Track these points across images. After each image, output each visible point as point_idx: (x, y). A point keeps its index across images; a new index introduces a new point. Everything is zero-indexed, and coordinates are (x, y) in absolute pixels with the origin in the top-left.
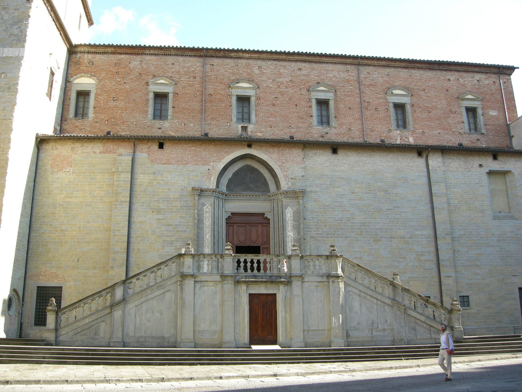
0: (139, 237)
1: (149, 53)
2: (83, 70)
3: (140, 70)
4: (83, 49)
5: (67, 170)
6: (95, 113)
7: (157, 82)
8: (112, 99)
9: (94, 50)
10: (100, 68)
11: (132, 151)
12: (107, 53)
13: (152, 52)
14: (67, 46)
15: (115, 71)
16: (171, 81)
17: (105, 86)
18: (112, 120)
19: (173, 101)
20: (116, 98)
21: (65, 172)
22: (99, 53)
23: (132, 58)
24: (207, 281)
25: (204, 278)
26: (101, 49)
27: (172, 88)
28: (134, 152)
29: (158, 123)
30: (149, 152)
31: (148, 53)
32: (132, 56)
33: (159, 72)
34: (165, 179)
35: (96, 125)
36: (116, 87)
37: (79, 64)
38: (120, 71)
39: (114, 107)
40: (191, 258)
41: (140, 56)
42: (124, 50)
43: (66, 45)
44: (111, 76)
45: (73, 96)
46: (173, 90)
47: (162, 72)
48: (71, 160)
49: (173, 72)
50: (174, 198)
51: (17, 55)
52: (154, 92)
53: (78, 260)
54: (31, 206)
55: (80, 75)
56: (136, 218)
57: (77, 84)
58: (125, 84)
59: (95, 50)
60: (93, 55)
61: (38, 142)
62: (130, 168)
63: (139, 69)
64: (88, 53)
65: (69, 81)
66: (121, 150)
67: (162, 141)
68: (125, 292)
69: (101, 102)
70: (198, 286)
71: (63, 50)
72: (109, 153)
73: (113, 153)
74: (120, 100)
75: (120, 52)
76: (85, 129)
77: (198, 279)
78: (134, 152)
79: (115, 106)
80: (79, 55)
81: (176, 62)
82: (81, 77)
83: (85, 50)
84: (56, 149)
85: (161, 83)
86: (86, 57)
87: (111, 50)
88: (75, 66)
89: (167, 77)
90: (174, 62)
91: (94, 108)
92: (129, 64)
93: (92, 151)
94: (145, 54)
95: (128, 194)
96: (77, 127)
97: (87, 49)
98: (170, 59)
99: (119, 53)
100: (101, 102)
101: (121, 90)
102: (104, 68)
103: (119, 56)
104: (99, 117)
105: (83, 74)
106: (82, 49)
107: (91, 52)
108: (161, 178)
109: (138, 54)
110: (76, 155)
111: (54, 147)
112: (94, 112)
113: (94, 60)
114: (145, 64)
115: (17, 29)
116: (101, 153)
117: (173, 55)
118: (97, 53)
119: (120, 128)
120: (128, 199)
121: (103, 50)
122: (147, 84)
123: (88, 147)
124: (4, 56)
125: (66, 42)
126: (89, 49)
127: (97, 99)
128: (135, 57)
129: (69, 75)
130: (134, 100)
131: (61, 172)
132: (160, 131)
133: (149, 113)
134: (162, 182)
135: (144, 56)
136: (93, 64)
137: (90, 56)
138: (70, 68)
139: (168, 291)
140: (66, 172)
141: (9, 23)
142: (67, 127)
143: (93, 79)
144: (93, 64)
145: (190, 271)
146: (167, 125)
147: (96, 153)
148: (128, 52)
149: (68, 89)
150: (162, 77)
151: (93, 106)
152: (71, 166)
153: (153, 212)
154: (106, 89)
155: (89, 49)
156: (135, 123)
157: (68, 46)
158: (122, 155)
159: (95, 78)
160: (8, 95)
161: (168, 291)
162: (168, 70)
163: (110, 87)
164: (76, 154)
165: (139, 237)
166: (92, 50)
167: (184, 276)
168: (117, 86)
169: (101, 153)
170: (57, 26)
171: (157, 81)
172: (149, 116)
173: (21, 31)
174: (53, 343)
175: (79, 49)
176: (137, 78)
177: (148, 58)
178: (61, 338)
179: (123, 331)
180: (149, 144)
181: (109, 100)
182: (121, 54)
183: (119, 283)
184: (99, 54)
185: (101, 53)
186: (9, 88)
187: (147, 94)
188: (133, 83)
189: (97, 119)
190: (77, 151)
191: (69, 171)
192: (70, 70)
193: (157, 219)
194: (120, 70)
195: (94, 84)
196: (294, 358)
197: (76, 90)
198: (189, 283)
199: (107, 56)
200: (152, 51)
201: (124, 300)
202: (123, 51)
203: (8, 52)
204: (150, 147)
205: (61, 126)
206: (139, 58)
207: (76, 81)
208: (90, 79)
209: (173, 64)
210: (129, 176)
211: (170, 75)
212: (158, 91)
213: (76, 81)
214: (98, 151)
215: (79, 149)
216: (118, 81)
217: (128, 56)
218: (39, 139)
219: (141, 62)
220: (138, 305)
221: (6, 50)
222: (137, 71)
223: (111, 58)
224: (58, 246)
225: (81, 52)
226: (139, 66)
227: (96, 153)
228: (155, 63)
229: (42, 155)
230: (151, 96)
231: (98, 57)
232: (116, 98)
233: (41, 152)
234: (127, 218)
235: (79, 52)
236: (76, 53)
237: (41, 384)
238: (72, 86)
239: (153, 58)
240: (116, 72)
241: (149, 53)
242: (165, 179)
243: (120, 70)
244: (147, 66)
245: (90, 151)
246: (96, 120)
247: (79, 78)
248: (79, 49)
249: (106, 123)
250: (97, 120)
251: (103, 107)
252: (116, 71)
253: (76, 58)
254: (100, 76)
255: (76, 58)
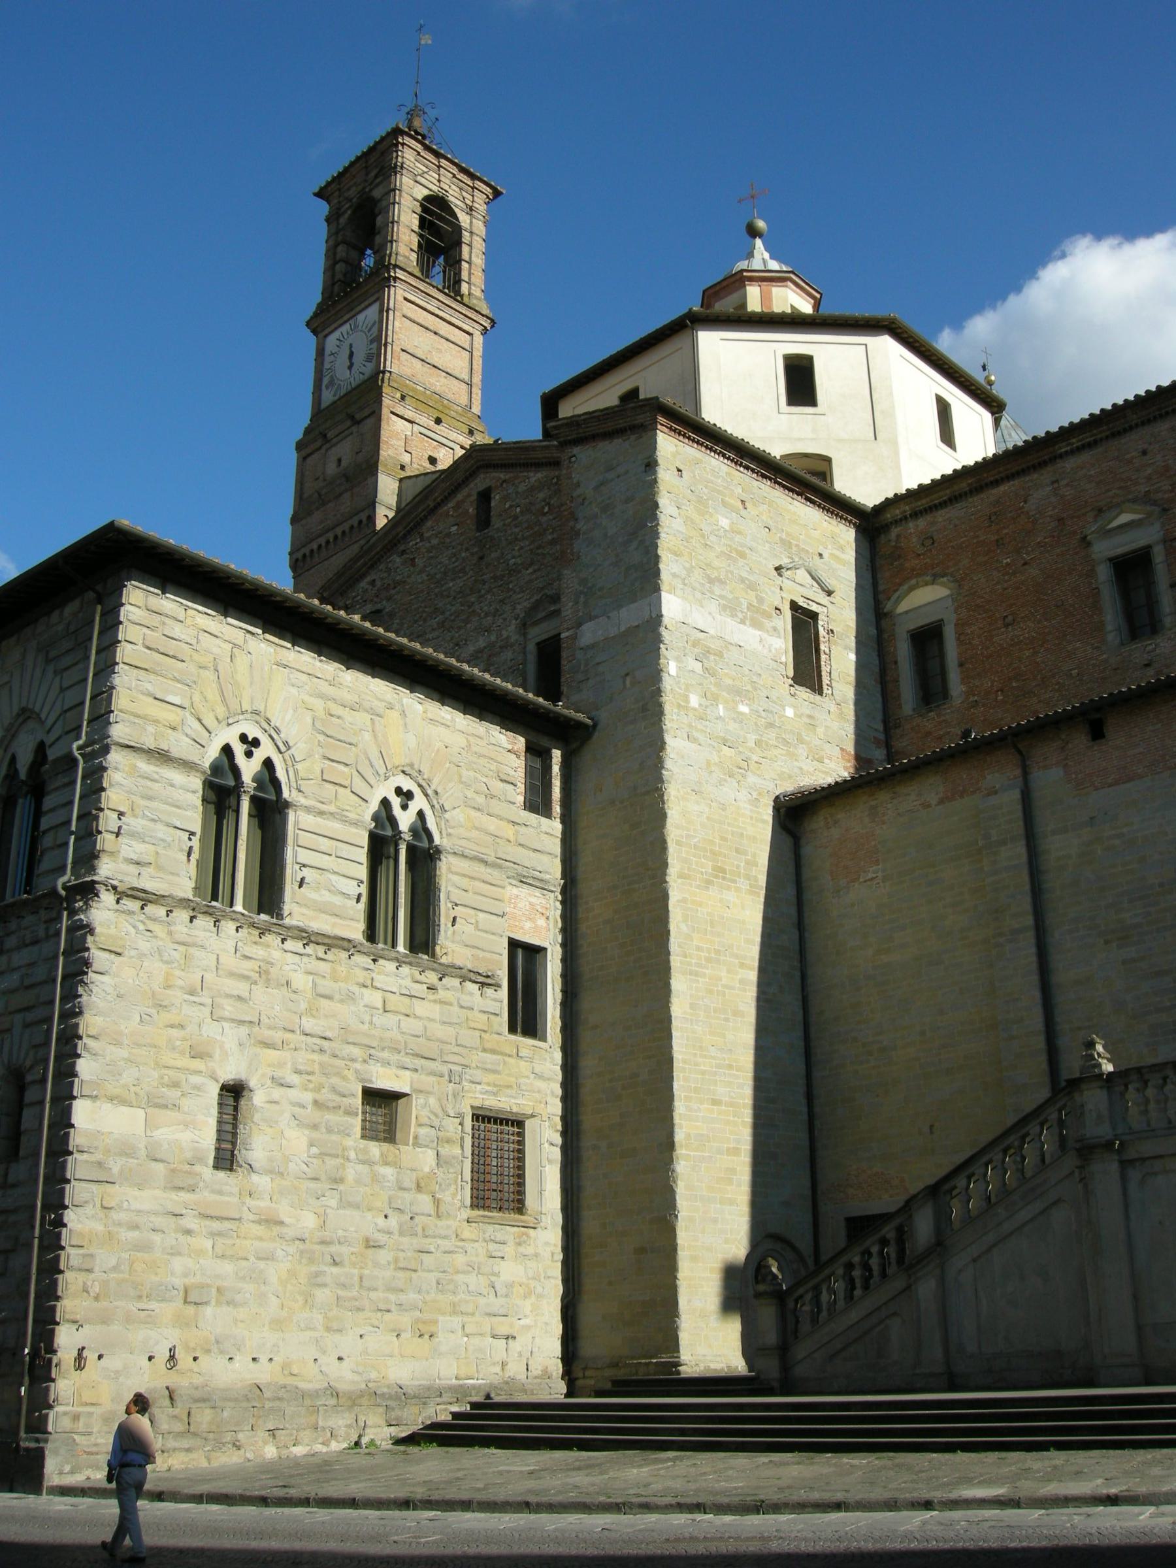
0: (1079, 1028)
1: (1069, 448)
2: (913, 570)
3: (1057, 511)
4: (897, 512)
5: (870, 875)
6: (965, 680)
7: (1111, 526)
8: (1000, 622)
9: (924, 501)
10: (953, 547)
11: (1018, 772)
12: (961, 496)
13: (1075, 442)
14: (850, 522)
15: (994, 538)
16: (1149, 508)
17: (976, 592)
18: (1014, 684)
19: (1168, 565)
20: (1010, 618)
21: (865, 881)
22: (940, 504)
23: (1030, 484)
24: (1161, 1157)
25: (1147, 1148)
26: (941, 494)
27: (1157, 526)
28: (1025, 774)
29: (1138, 651)
30: (1066, 759)
31: (1066, 452)
32: (1027, 479)
33: (1111, 494)
34: (1125, 830)
35: (974, 713)
36: (1005, 585)
37: (899, 556)
38: (1007, 534)
39: (1012, 645)
40: (1101, 1088)
41: (1050, 468)
42: (1001, 469)
43: (846, 519)
44: (986, 558)
45: (903, 650)
46: (1162, 533)
47: (1120, 488)
48: (873, 843)
49: (1149, 478)
50: (1161, 885)
51: (647, 617)
52: (1110, 560)
53: (932, 1127)
54: (800, 997)
55: (905, 587)
56: (1065, 974)
57: (906, 612)
58: (1026, 567)
59: (928, 499)
60: (929, 517)
61: (782, 818)
62: (1021, 823)
63: (1054, 508)
64: (916, 515)
65: (886, 614)
66: (989, 777)
67: (1098, 716)
68: (942, 1218)
69: (974, 642)
70: (1135, 1175)
71: (846, 535)
72: (962, 796)
73: (974, 792)
74: (1022, 618)
75: (992, 479)
76: (949, 733)
77: (1131, 1153)
78: (1025, 774)
79: (1012, 640)
80: (894, 532)
81: (1150, 444)
82: (912, 589)
83: (905, 512)
84: (836, 822)
85: (1121, 527)
86: (912, 531)
87: (969, 485)
88: (892, 564)
89: (1134, 501)
90: (1146, 446)
91: (961, 665)
92: (1025, 502)
93: (918, 802)
94: (1061, 456)
95: (1026, 904)
96: (929, 733)
97: (907, 508)
98: (1133, 442)
99: (992, 483)
100: (974, 642)
101: (1018, 588)
102: (963, 542)
103: (994, 491)
104: (977, 686)
105: (913, 582)
106: (897, 512)
107: (921, 512)
108: (1113, 832)
109: (1042, 464)
110: (884, 827)
111: (829, 820)
112: (963, 679)
113: (934, 529)
114: (1067, 485)
115: (636, 549)
116: (941, 802)
117: (1137, 425)
118: (935, 506)
119: (1040, 702)
120: (1030, 921)
121: (948, 492)
122: (1085, 542)
123: (909, 794)
124: (623, 629)
125: (841, 513)
126: (913, 505)
127: (962, 638)
128: (1035, 476)
129: (881, 597)
130: (1060, 603)
131: (857, 885)
132: (1151, 672)
133: (1109, 628)
134: (1117, 842)
135: (1060, 464)
136: (933, 543)
137: (922, 523)
138: (879, 576)
139: (1055, 1203)
140: (868, 883)
141: (620, 540)
142: (904, 744)
143: (943, 585)
144: (933, 543)
145: (1103, 1131)
146: (1165, 647)
147: (929, 806)
148: (1013, 471)
149: (886, 636)
150: (1117, 507)
151: (956, 663)
152: (877, 862)
153: (1107, 942)
154: (979, 601)
155: (913, 505)
156: (1074, 672)
157: (854, 520)
158: (996, 793)
159: (945, 579)
160: (645, 728)
161: (1055, 1203)
162: (1133, 477)
163: (988, 590)
164: (884, 823)
165: (1079, 1028)
166: (919, 503)
167: (1087, 1151)
168: (1008, 581)
169: (941, 802)
170: (784, 487)
171: (1108, 524)
172: (1110, 637)
173: (647, 552)
174: (775, 1384)
175: (888, 516)
176: (1054, 537)
177: (1070, 464)
178: (800, 1371)
179: (946, 1341)
180: (1063, 737)
181: (994, 630)
182: (996, 483)
183: (920, 1196)
184: (942, 508)
185: (945, 502)
186: (644, 709)
187: (1092, 573)
188: (1047, 555)
189: (974, 695)
190: (884, 814)
191: (874, 875)
192: (880, 582)
193: (1124, 962)
194: (1005, 531)
195: (948, 596)
196: (1004, 1413)
197: (908, 632)
198: (1106, 1171)
199: (964, 504)
200: (1074, 440)
201: (940, 1245)
202: (999, 472)
203: (628, 616)
204: (1067, 743)
205: (888, 746)
206: (1045, 476)
207: (903, 607)
208: (936, 587)
209: (1144, 453)
210: (1021, 849)
211: (1143, 489)
212: (1120, 551)
213: (903, 607)
214: (933, 799)
215: (889, 806)
216: (1008, 564)
217: (1016, 482)
218: (783, 811)
219: (1056, 485)
220: (979, 1257)
221: (624, 612)
222: (1051, 516)
223: (974, 507)
224: (878, 1096)
225: (896, 521)
226: (1053, 499)
227: (929, 806)
228: (1092, 472)
229: (807, 850)
230: (1104, 573)
231: (941, 516)
232: (1010, 618)
233: (803, 842)
234: (1035, 978)
235: (891, 523)
236: (886, 528)
237: (473, 1511)
238: (894, 625)
239: (1085, 457)
240: (997, 541)
241: (1069, 448)
242: (1125, 830)
243: (1005, 531)
244: (1072, 492)
245: (915, 803)
246: (971, 699)
247: (906, 595)
248: (888, 516)
249: (1000, 698)
250: (976, 698)
251: (982, 653)
252: (996, 537)
253: (890, 541)
254: (959, 569)
255: (890, 541)
